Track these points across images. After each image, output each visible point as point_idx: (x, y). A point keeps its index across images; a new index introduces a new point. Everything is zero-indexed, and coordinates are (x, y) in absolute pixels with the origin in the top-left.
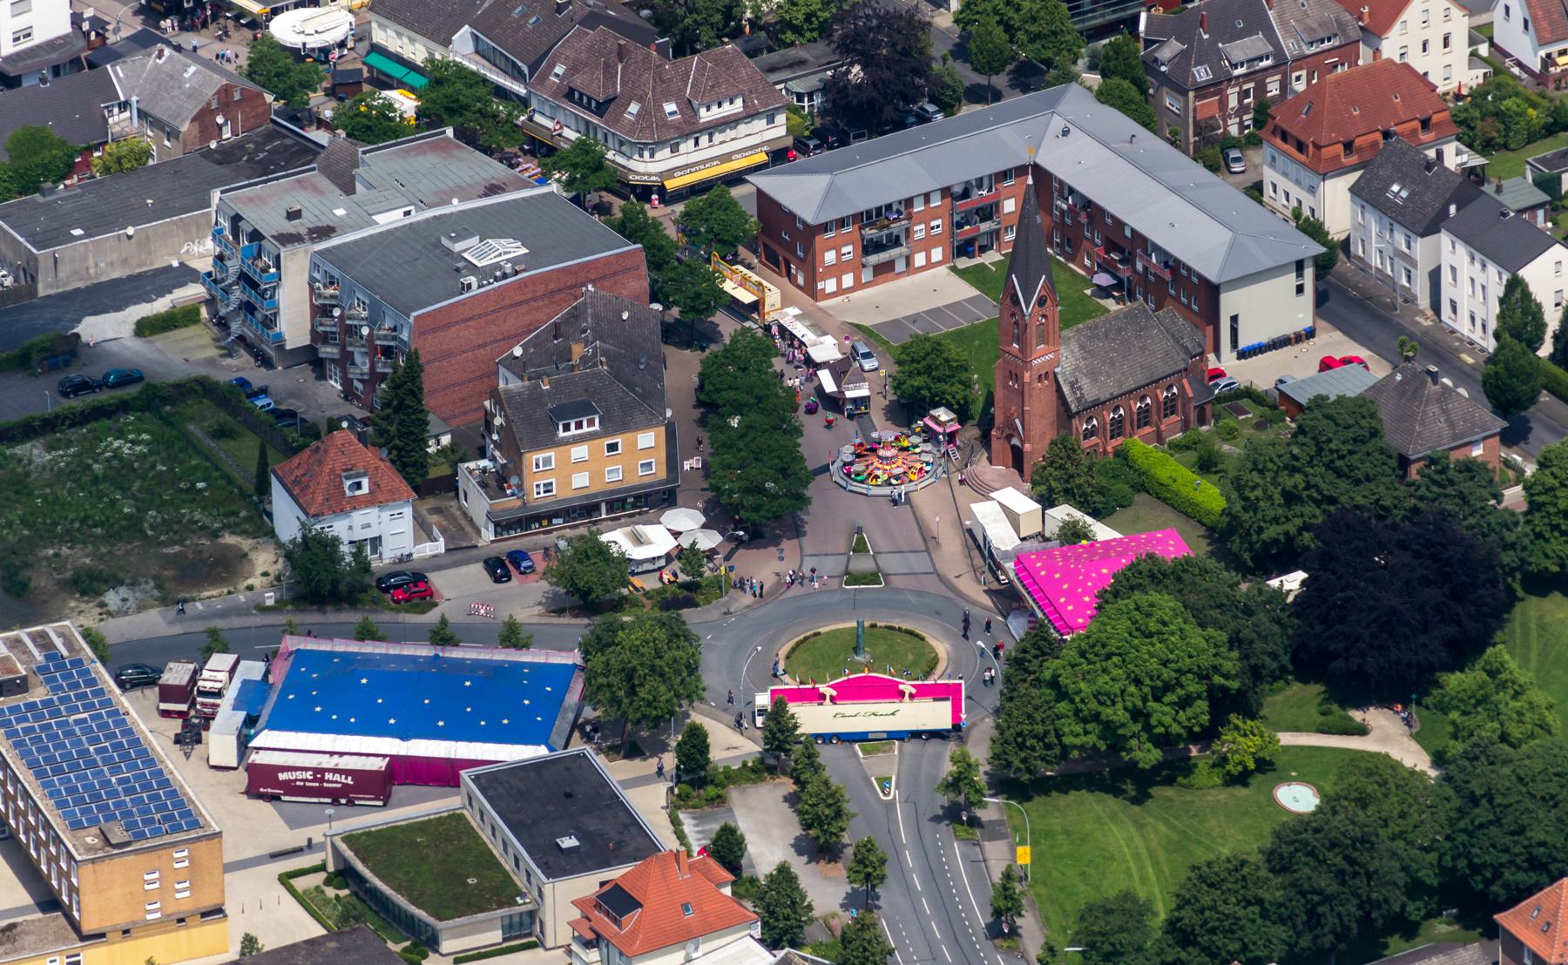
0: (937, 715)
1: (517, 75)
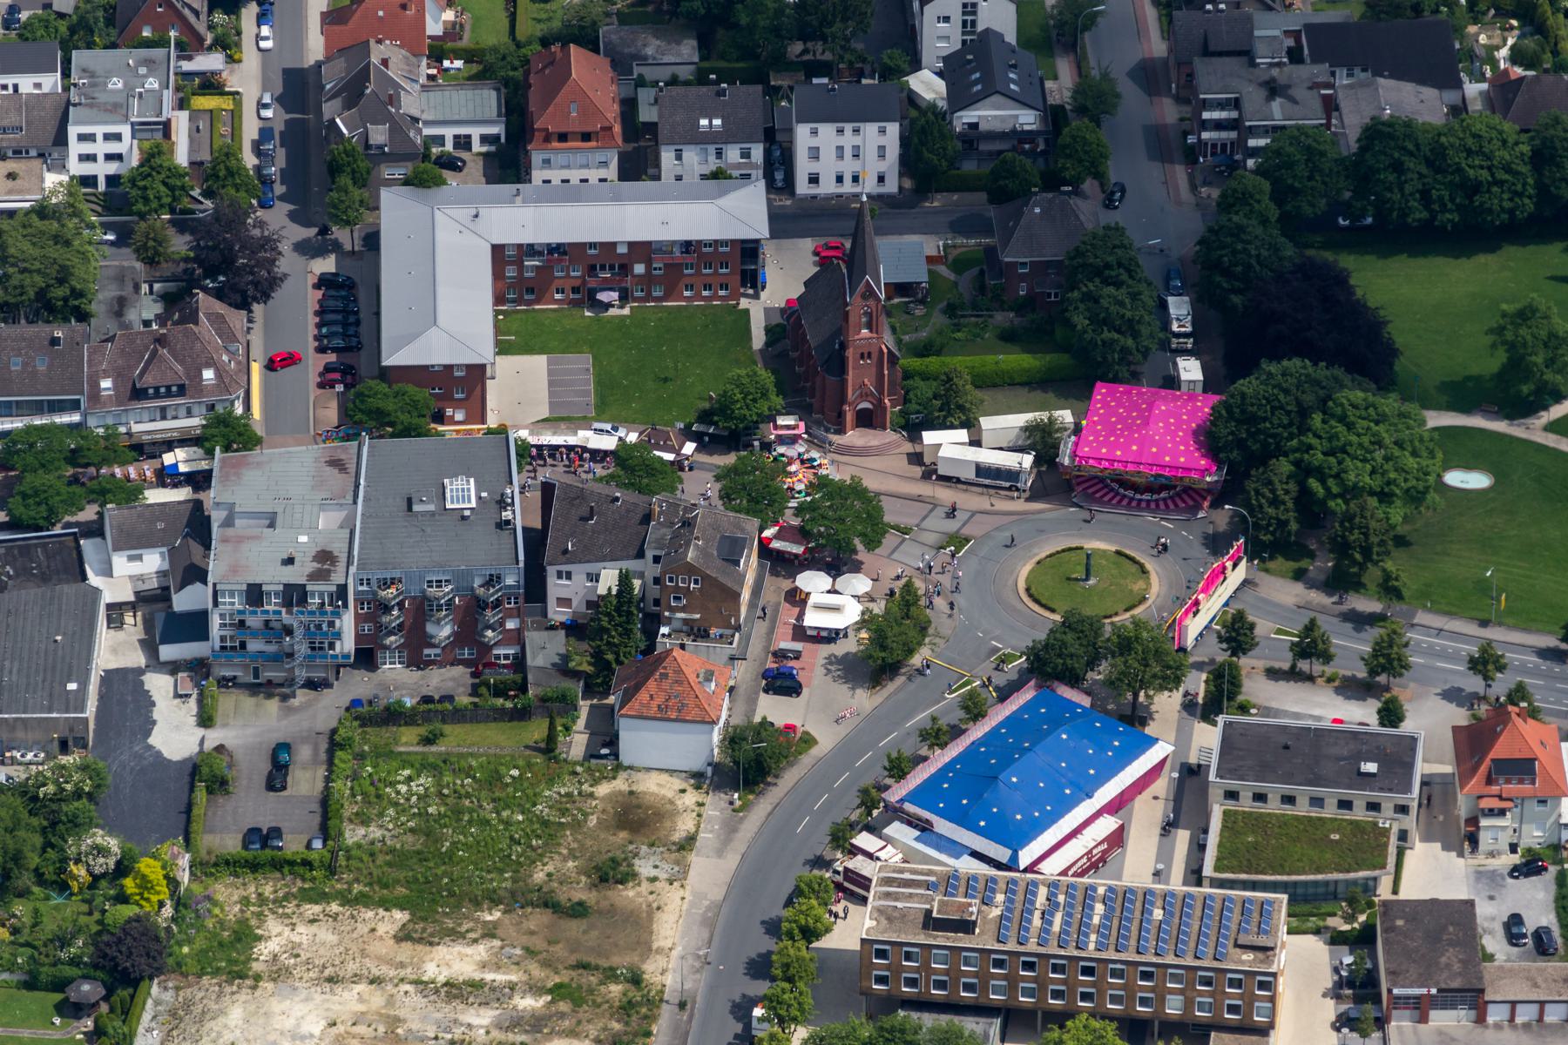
0: (1236, 576)
1: (75, 406)
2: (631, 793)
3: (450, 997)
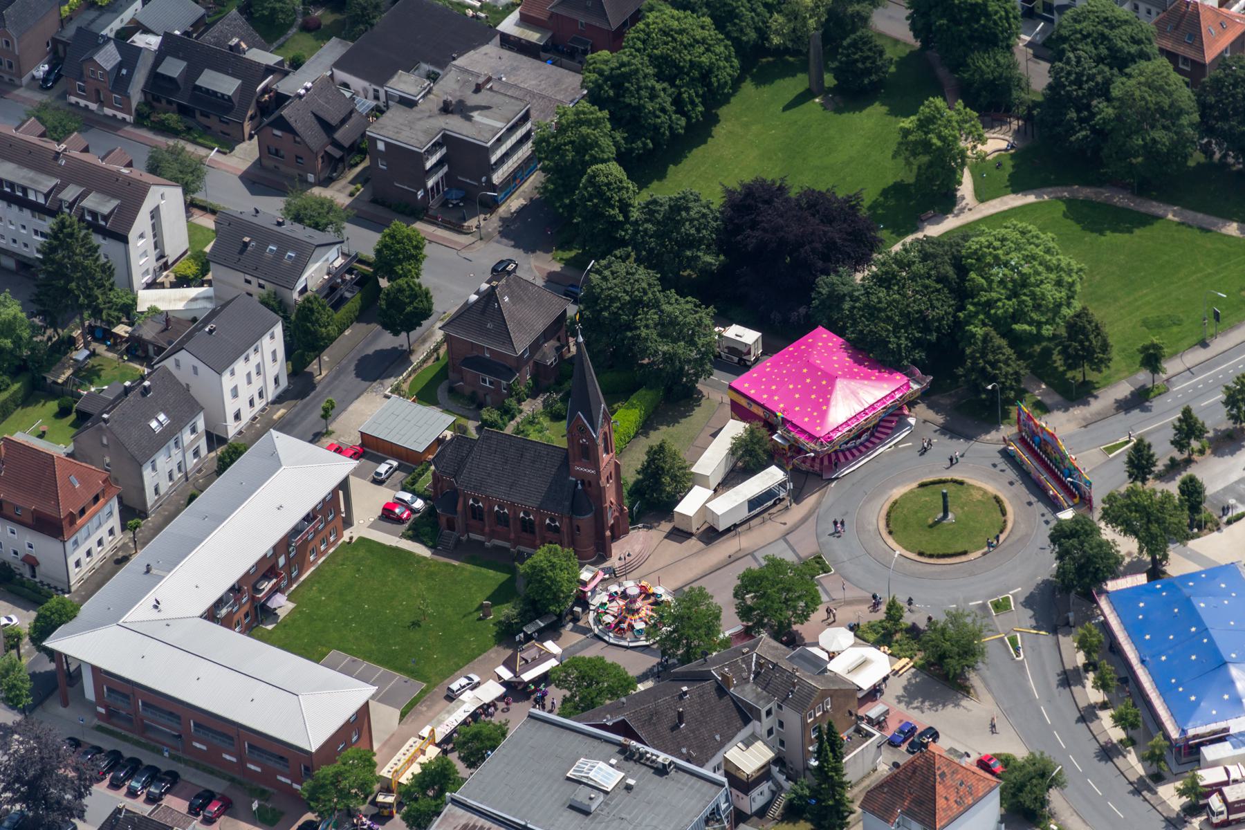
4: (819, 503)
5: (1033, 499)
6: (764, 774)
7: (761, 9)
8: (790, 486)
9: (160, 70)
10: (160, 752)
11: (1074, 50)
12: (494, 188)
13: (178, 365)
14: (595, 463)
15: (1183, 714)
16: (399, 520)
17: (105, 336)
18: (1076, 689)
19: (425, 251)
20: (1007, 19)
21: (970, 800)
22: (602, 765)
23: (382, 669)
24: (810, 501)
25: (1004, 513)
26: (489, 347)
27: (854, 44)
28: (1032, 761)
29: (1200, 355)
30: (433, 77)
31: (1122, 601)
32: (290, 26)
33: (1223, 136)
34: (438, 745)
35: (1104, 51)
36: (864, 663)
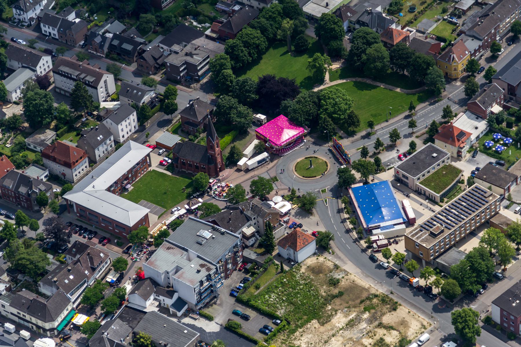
2: (308, 267)
3: (352, 326)
4: (277, 163)
5: (336, 162)
6: (253, 235)
7: (274, 28)
8: (269, 158)
9: (112, 43)
10: (92, 226)
11: (357, 40)
12: (198, 76)
13: (107, 122)
14: (214, 151)
15: (368, 221)
16: (164, 165)
17: (91, 114)
18: (341, 214)
19: (178, 93)
20: (341, 32)
21: (307, 243)
22: (206, 232)
23: (155, 205)
24: (275, 162)
25: (327, 166)
26: (192, 119)
27: (299, 38)
28: (326, 233)
29: (386, 124)
30: (185, 46)
31: (355, 190)
32: (150, 31)
33: (396, 64)
34: (167, 226)
35: (365, 41)
36: (284, 206)
